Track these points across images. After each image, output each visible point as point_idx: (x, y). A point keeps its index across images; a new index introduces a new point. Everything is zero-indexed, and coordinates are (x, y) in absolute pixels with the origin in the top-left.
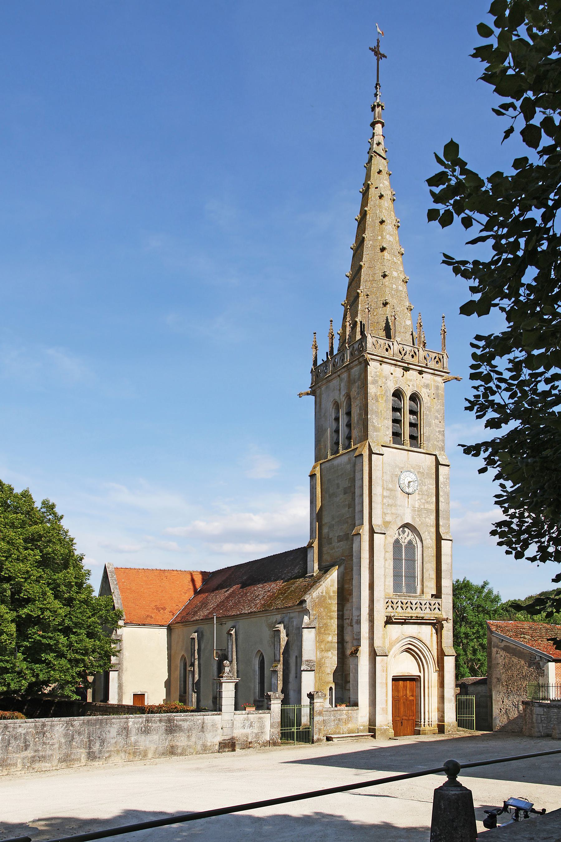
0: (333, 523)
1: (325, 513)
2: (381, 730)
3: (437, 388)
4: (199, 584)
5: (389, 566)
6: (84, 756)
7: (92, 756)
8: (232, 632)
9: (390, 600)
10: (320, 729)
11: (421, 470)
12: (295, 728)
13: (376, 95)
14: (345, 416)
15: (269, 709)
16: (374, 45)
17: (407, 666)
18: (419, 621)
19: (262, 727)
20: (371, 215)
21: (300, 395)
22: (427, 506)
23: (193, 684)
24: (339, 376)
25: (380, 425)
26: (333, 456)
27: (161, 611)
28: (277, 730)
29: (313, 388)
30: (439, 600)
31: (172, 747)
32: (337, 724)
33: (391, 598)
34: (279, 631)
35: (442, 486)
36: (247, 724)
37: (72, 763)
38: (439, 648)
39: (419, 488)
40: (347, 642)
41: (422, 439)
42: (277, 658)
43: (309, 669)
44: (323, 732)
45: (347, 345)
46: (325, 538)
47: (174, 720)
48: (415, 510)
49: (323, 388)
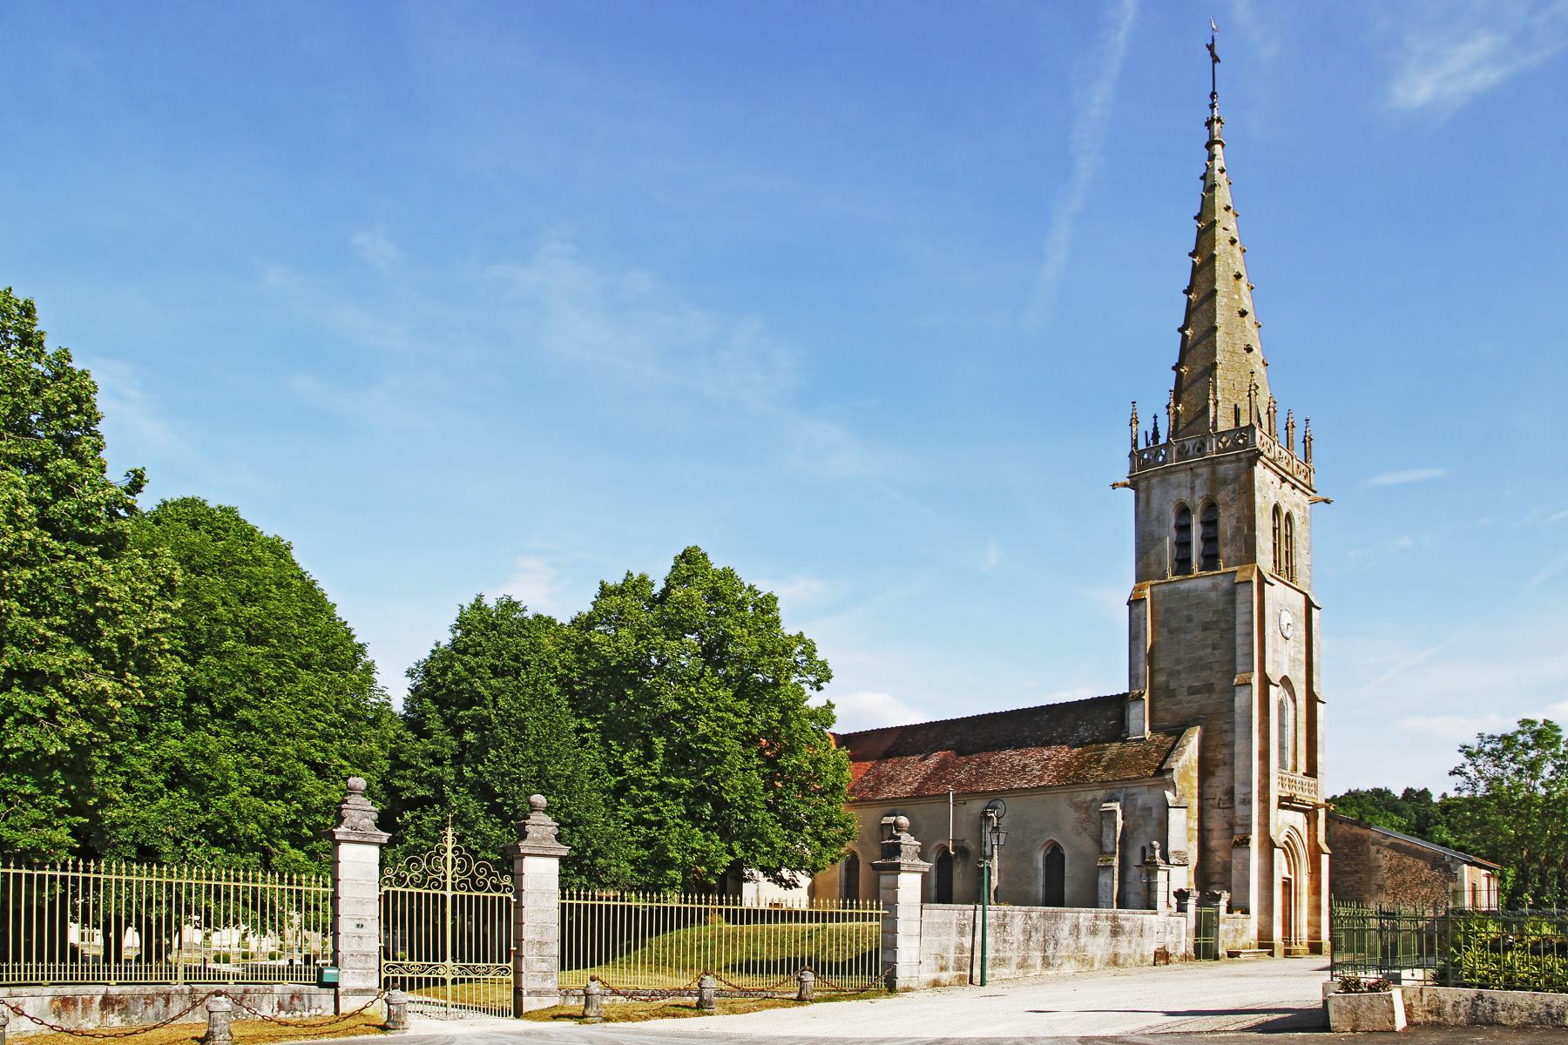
1: (1158, 654)
6: (1039, 961)
7: (1047, 963)
13: (1212, 106)
21: (1114, 486)
42: (1110, 848)
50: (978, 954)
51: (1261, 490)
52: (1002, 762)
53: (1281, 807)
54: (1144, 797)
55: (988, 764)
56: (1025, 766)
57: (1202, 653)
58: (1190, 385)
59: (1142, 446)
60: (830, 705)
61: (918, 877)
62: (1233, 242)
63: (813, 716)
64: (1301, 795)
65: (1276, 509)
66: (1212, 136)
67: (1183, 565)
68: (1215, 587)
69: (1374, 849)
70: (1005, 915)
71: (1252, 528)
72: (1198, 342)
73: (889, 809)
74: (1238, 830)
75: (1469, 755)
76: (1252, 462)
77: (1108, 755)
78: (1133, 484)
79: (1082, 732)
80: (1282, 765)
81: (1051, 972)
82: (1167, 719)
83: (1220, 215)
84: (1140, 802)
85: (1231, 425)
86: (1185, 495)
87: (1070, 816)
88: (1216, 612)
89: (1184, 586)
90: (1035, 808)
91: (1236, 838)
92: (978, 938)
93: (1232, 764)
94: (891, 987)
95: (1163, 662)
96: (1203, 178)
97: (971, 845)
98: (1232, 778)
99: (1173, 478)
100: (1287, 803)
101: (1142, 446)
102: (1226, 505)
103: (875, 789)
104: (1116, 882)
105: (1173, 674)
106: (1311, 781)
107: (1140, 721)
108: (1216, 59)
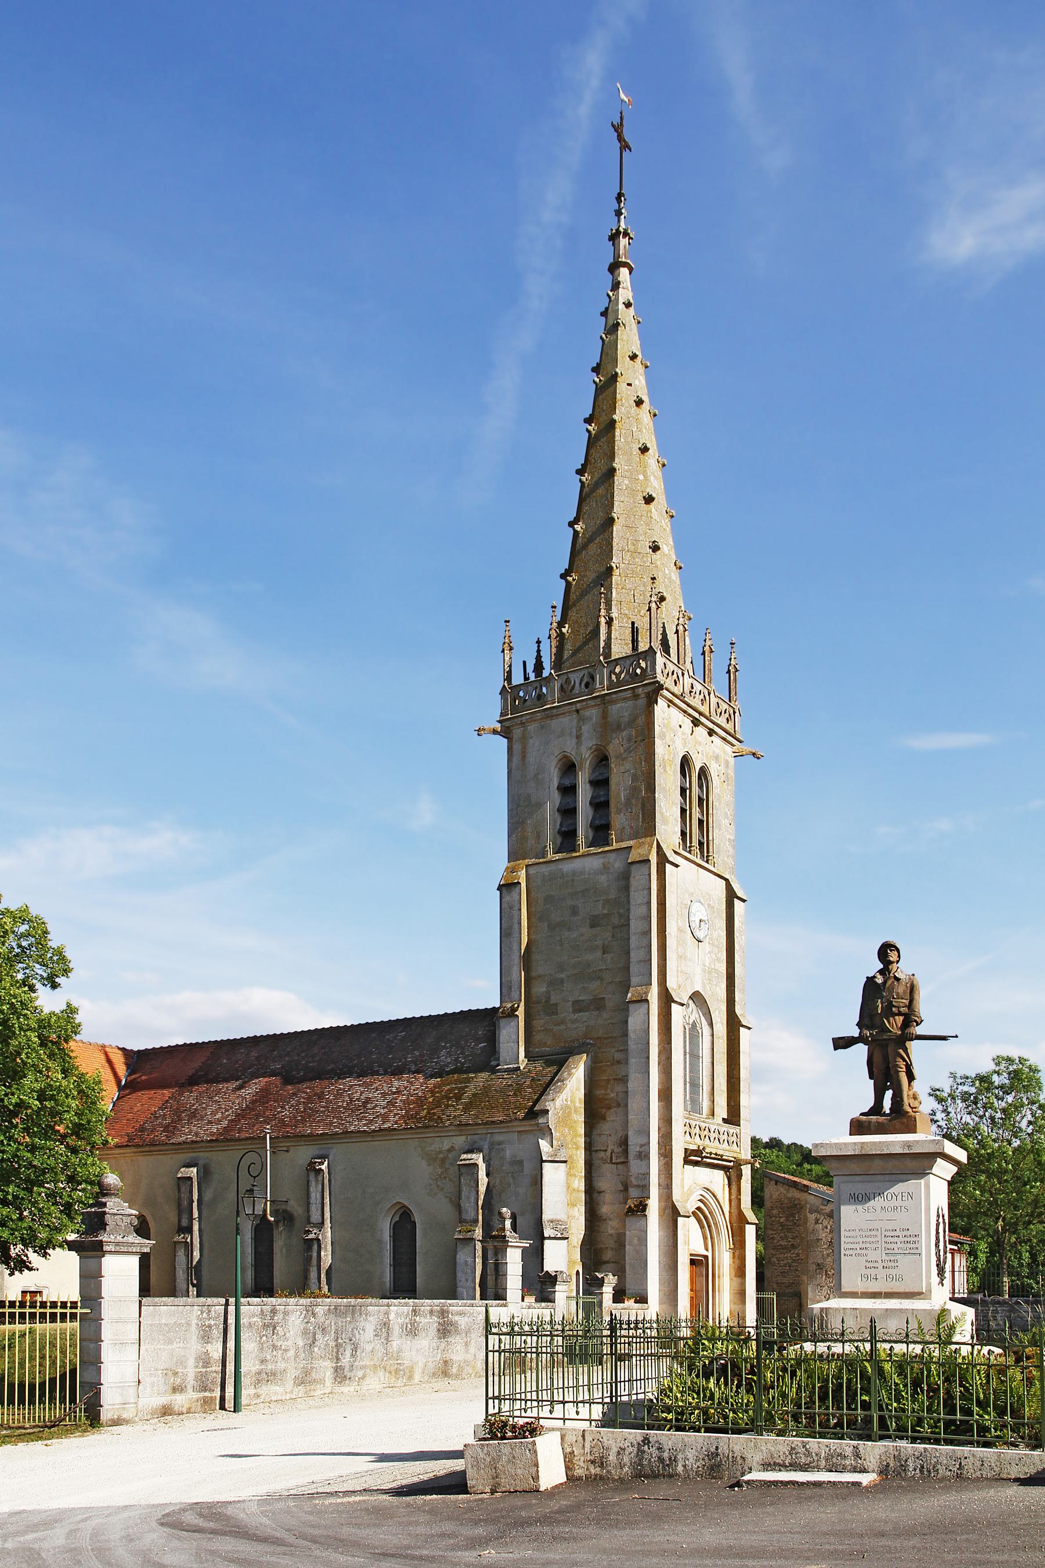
0: (563, 976)
1: (535, 957)
4: (122, 1070)
6: (329, 1374)
7: (340, 1375)
8: (324, 1167)
13: (618, 213)
14: (588, 785)
16: (617, 121)
18: (716, 1162)
20: (623, 431)
21: (479, 732)
23: (189, 1267)
26: (558, 856)
29: (507, 724)
31: (446, 1362)
34: (476, 1165)
37: (313, 1387)
38: (735, 1211)
40: (600, 1192)
41: (711, 850)
42: (470, 1215)
43: (559, 1235)
45: (601, 658)
46: (538, 1002)
47: (448, 1312)
49: (532, 727)
50: (230, 1367)
51: (663, 737)
52: (339, 1094)
53: (687, 1161)
54: (513, 1148)
55: (321, 1096)
56: (368, 1100)
57: (589, 957)
58: (578, 600)
59: (518, 679)
60: (71, 1010)
61: (135, 1261)
62: (639, 403)
63: (44, 1024)
64: (712, 1147)
65: (685, 763)
66: (616, 255)
67: (567, 839)
68: (606, 867)
69: (812, 1217)
70: (274, 1312)
71: (651, 789)
72: (591, 540)
73: (186, 1157)
74: (634, 1193)
75: (940, 1100)
76: (652, 701)
77: (471, 1089)
78: (506, 732)
79: (445, 1058)
80: (694, 1105)
81: (347, 1389)
82: (548, 1044)
83: (623, 366)
84: (508, 1154)
85: (628, 650)
86: (569, 746)
87: (422, 1171)
88: (606, 902)
89: (567, 867)
90: (312, 1166)
91: (631, 1203)
92: (231, 1344)
93: (626, 1105)
94: (93, 1418)
95: (540, 968)
96: (605, 314)
97: (295, 1207)
98: (626, 1122)
99: (554, 723)
100: (694, 1158)
101: (518, 679)
102: (619, 757)
103: (170, 1129)
104: (479, 1261)
105: (555, 983)
106: (732, 1129)
107: (514, 1048)
108: (625, 146)
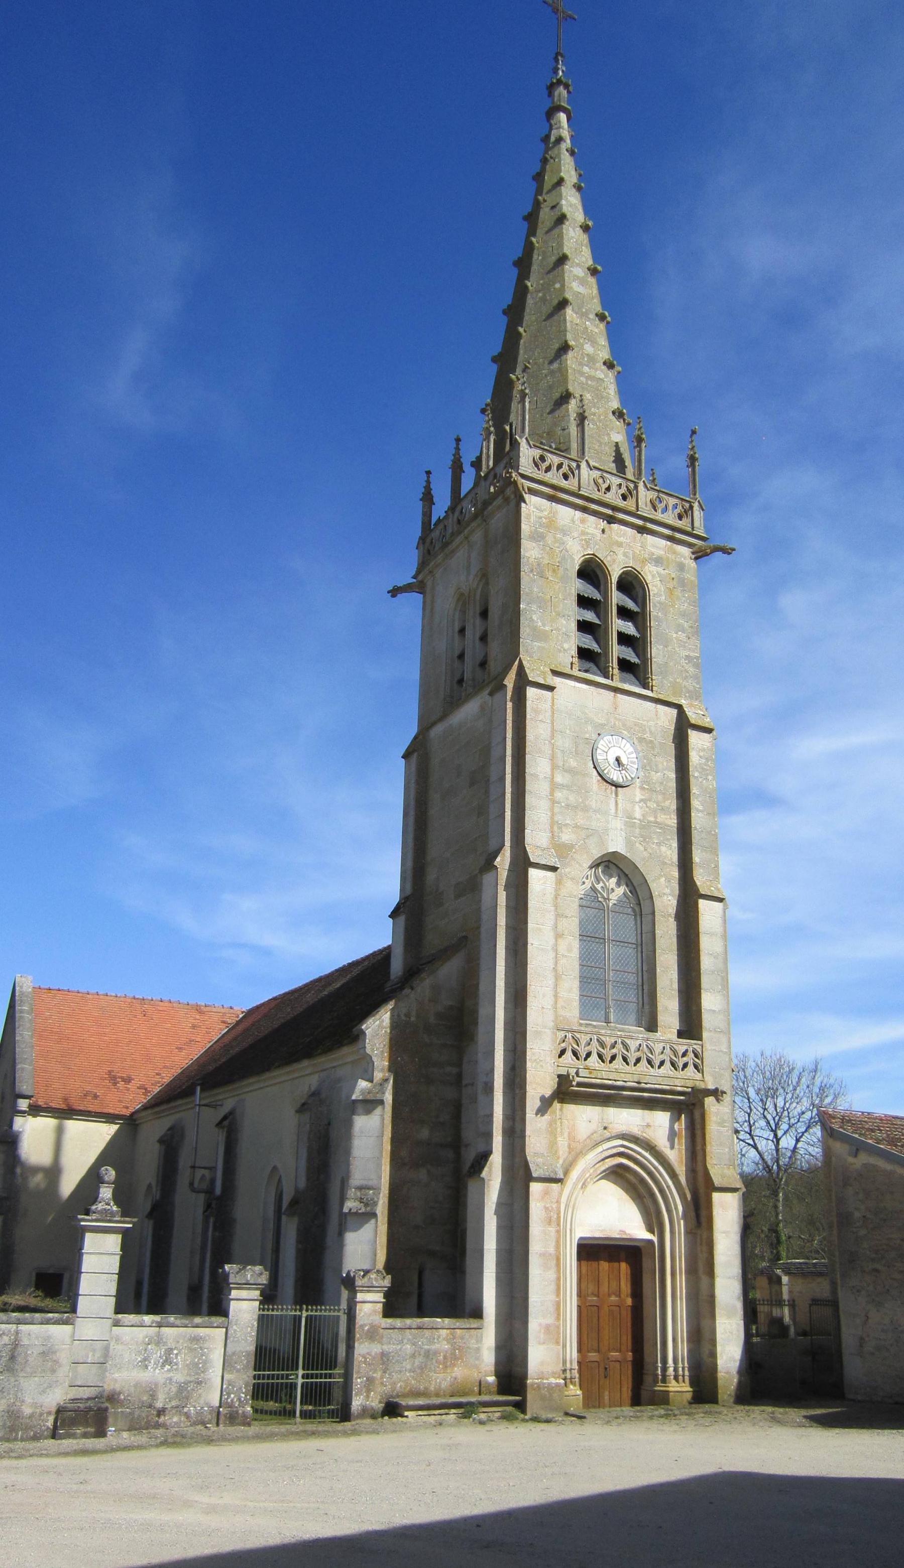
2: (539, 1387)
3: (681, 567)
5: (570, 950)
9: (569, 1035)
10: (370, 1381)
11: (647, 736)
12: (301, 1372)
15: (225, 1313)
17: (614, 1215)
19: (199, 1368)
22: (662, 818)
24: (466, 538)
25: (549, 628)
27: (121, 1084)
28: (243, 1378)
29: (420, 577)
30: (694, 1044)
32: (421, 1368)
33: (573, 1031)
35: (696, 774)
36: (157, 1354)
39: (641, 774)
44: (380, 1389)
48: (633, 825)
